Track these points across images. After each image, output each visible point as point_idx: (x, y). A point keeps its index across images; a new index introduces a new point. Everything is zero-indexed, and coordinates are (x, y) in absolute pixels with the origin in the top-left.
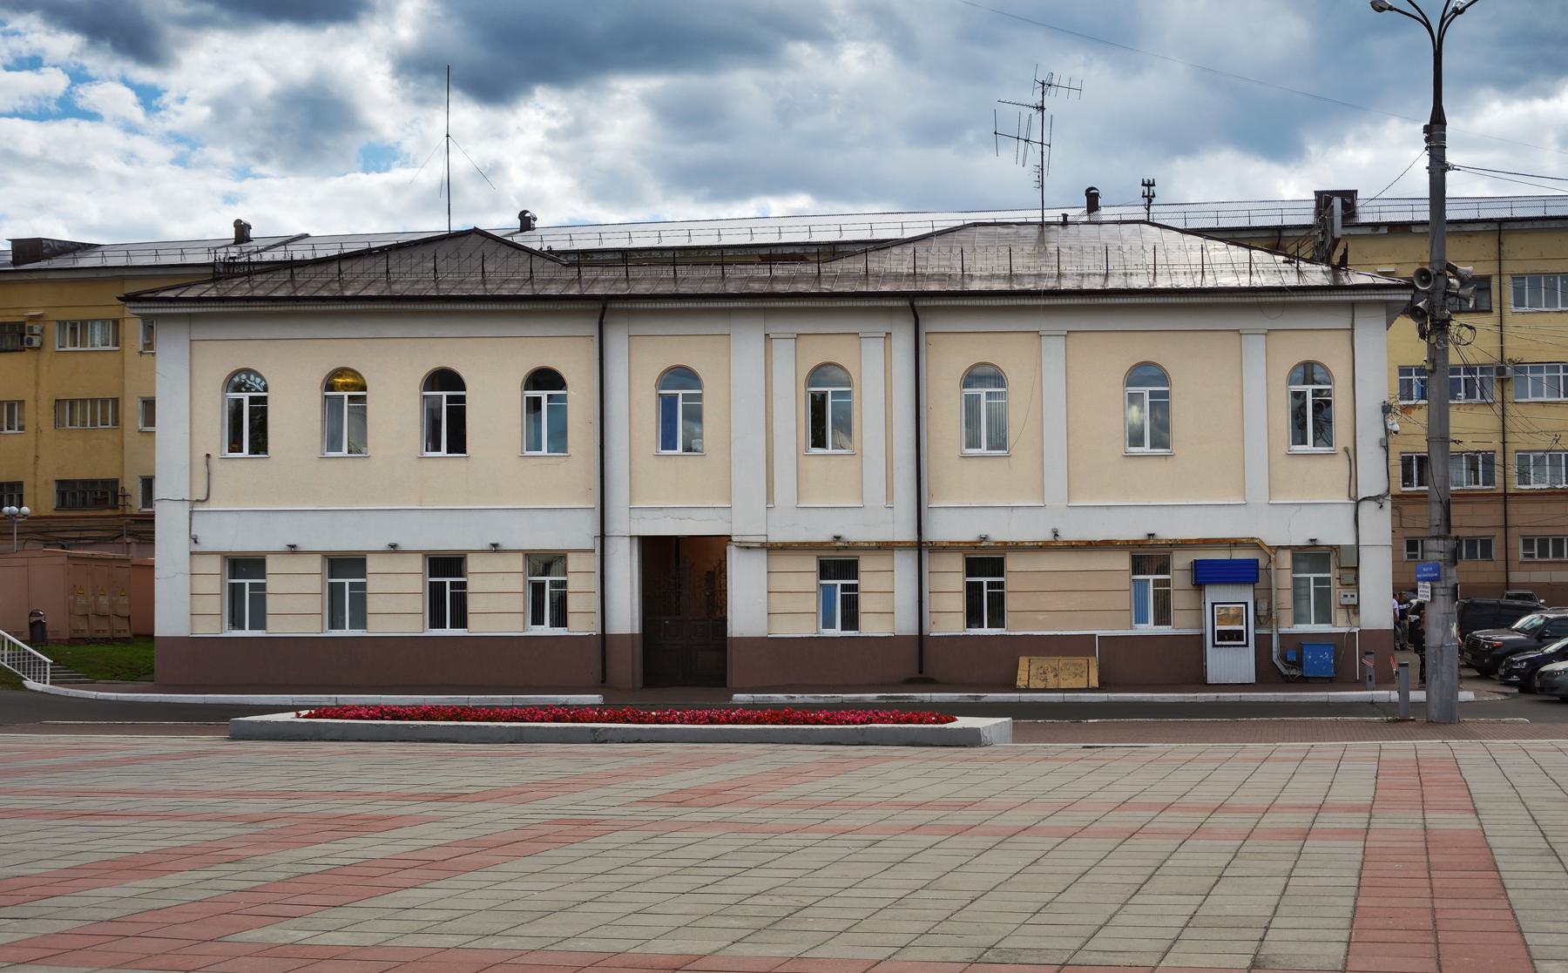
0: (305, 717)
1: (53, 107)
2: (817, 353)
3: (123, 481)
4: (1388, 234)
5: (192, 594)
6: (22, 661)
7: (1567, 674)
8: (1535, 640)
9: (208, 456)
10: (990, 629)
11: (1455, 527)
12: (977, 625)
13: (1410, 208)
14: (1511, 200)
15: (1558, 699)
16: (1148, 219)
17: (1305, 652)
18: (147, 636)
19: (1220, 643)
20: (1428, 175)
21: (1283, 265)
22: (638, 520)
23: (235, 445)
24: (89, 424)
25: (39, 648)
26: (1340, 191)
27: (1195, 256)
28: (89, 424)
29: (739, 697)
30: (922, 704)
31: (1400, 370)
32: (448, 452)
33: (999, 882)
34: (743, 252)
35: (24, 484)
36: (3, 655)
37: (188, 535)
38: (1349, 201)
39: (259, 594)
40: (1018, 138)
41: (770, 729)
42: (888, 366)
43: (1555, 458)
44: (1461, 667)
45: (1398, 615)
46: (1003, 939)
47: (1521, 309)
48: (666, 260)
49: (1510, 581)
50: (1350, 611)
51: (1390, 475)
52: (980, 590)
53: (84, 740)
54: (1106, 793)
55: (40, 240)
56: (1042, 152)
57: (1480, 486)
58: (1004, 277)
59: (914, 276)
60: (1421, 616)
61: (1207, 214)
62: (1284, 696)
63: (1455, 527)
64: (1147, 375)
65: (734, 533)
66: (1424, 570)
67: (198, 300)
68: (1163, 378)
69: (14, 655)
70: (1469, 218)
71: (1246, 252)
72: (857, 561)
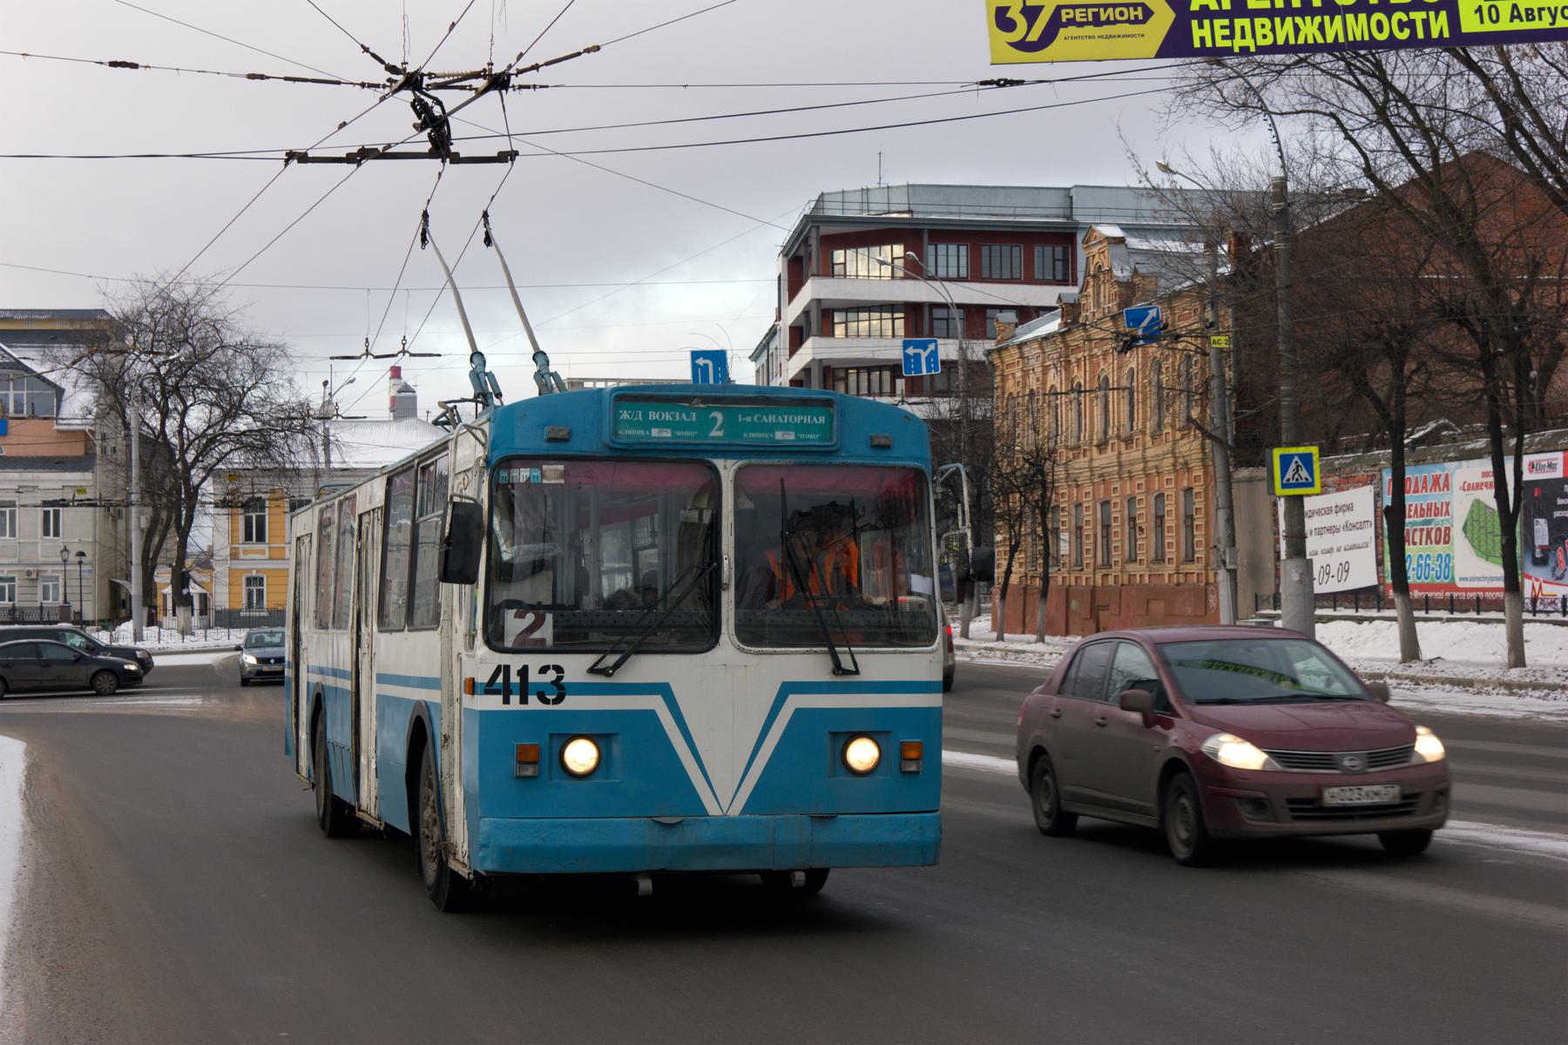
0: (1311, 473)
3: (233, 531)
4: (834, 310)
5: (881, 336)
8: (1031, 448)
9: (1143, 35)
16: (42, 618)
20: (370, 161)
22: (517, 75)
23: (46, 533)
24: (8, 514)
25: (974, 510)
27: (403, 542)
28: (8, 514)
30: (761, 431)
32: (378, 696)
34: (567, 648)
35: (729, 355)
36: (1330, 9)
37: (1320, 497)
38: (153, 611)
39: (260, 593)
40: (509, 135)
45: (446, 535)
53: (1221, 633)
54: (1404, 691)
58: (1490, 377)
61: (65, 422)
62: (1031, 331)
63: (1486, 485)
64: (1366, 545)
68: (1144, 21)
71: (836, 326)
72: (1075, 234)
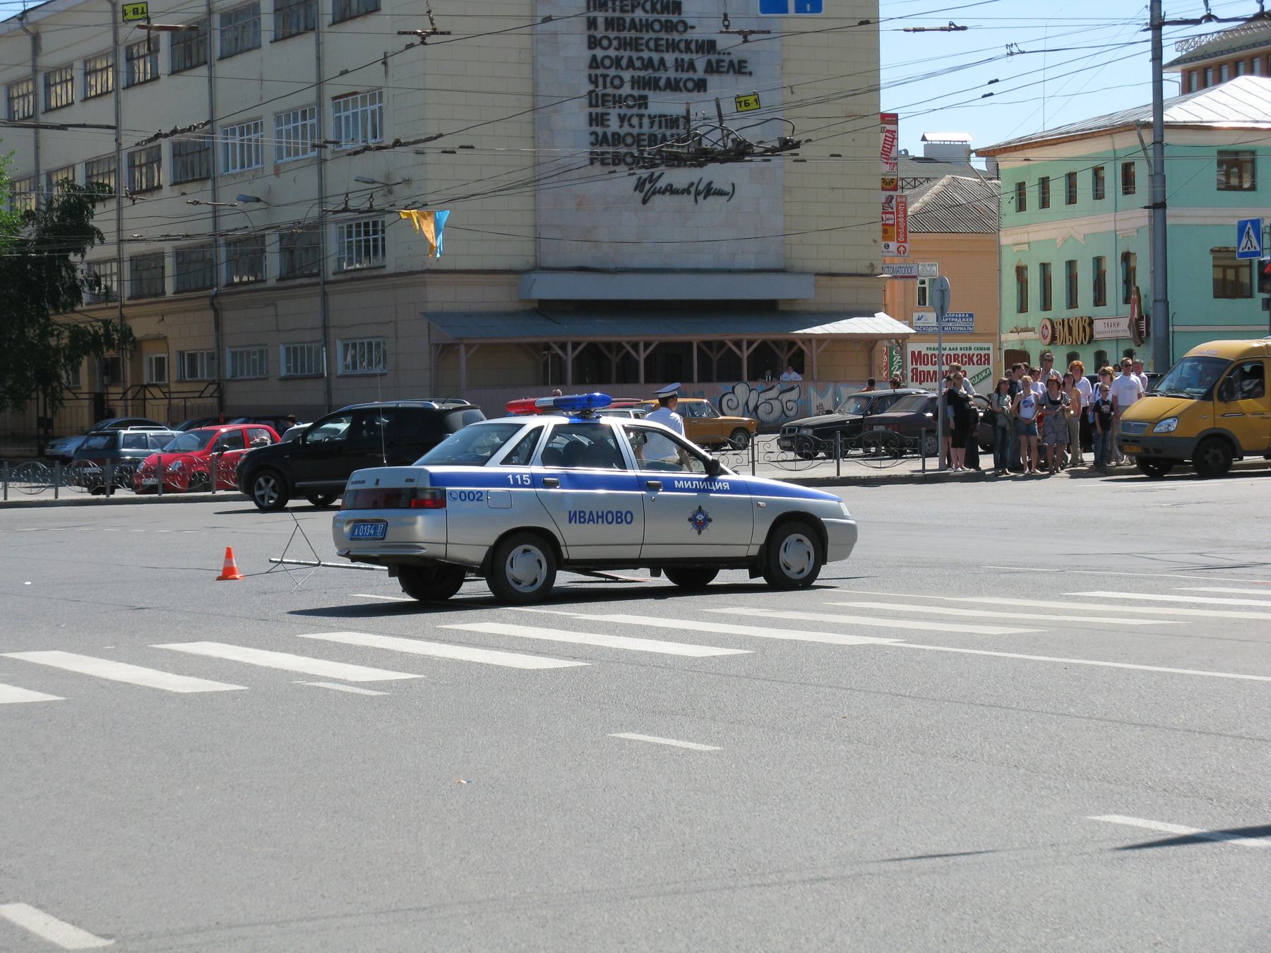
1: (1099, 193)
2: (378, 487)
6: (363, 238)
7: (1108, 952)
10: (790, 10)
11: (36, 133)
12: (1025, 272)
13: (533, 188)
14: (184, 395)
15: (664, 581)
17: (445, 216)
18: (1098, 262)
19: (167, 379)
21: (1111, 854)
26: (1174, 61)
29: (1247, 459)
31: (1070, 308)
33: (357, 156)
41: (895, 418)
42: (1160, 270)
43: (653, 144)
44: (697, 41)
46: (920, 857)
47: (368, 340)
48: (12, 115)
49: (922, 155)
50: (520, 483)
51: (450, 88)
52: (823, 549)
55: (781, 515)
56: (915, 30)
57: (299, 373)
59: (430, 369)
60: (665, 89)
65: (552, 14)
66: (882, 428)
67: (141, 182)
69: (375, 232)
70: (477, 650)
